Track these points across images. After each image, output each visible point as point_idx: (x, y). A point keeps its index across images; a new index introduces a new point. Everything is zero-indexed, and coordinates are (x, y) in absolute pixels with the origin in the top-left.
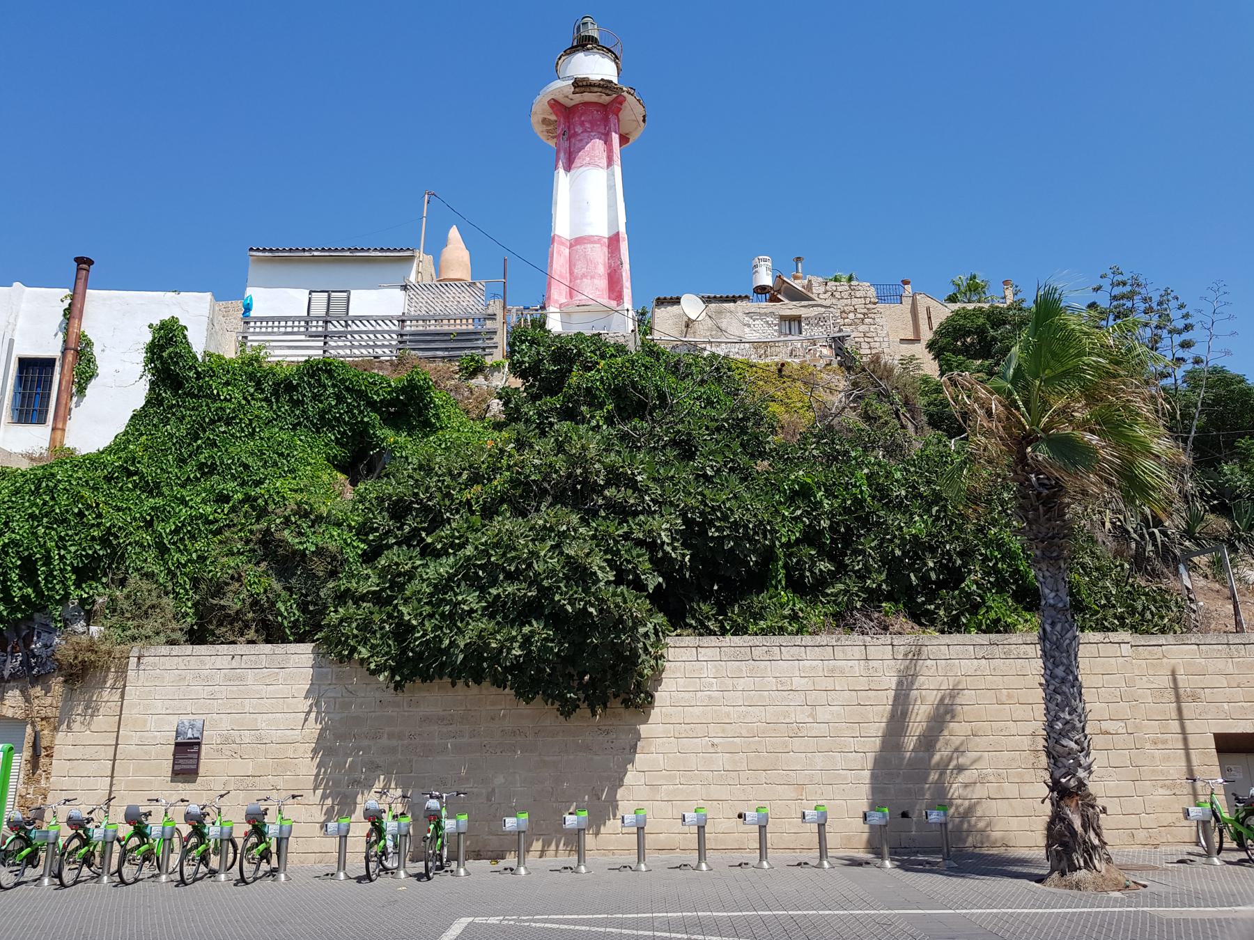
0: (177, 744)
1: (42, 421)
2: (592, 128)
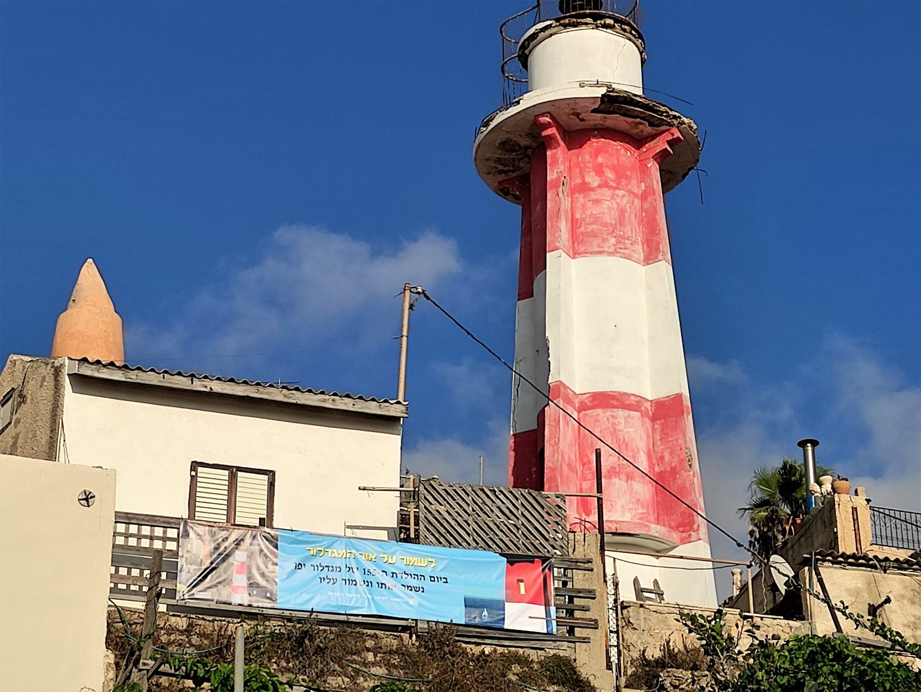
2: (618, 180)
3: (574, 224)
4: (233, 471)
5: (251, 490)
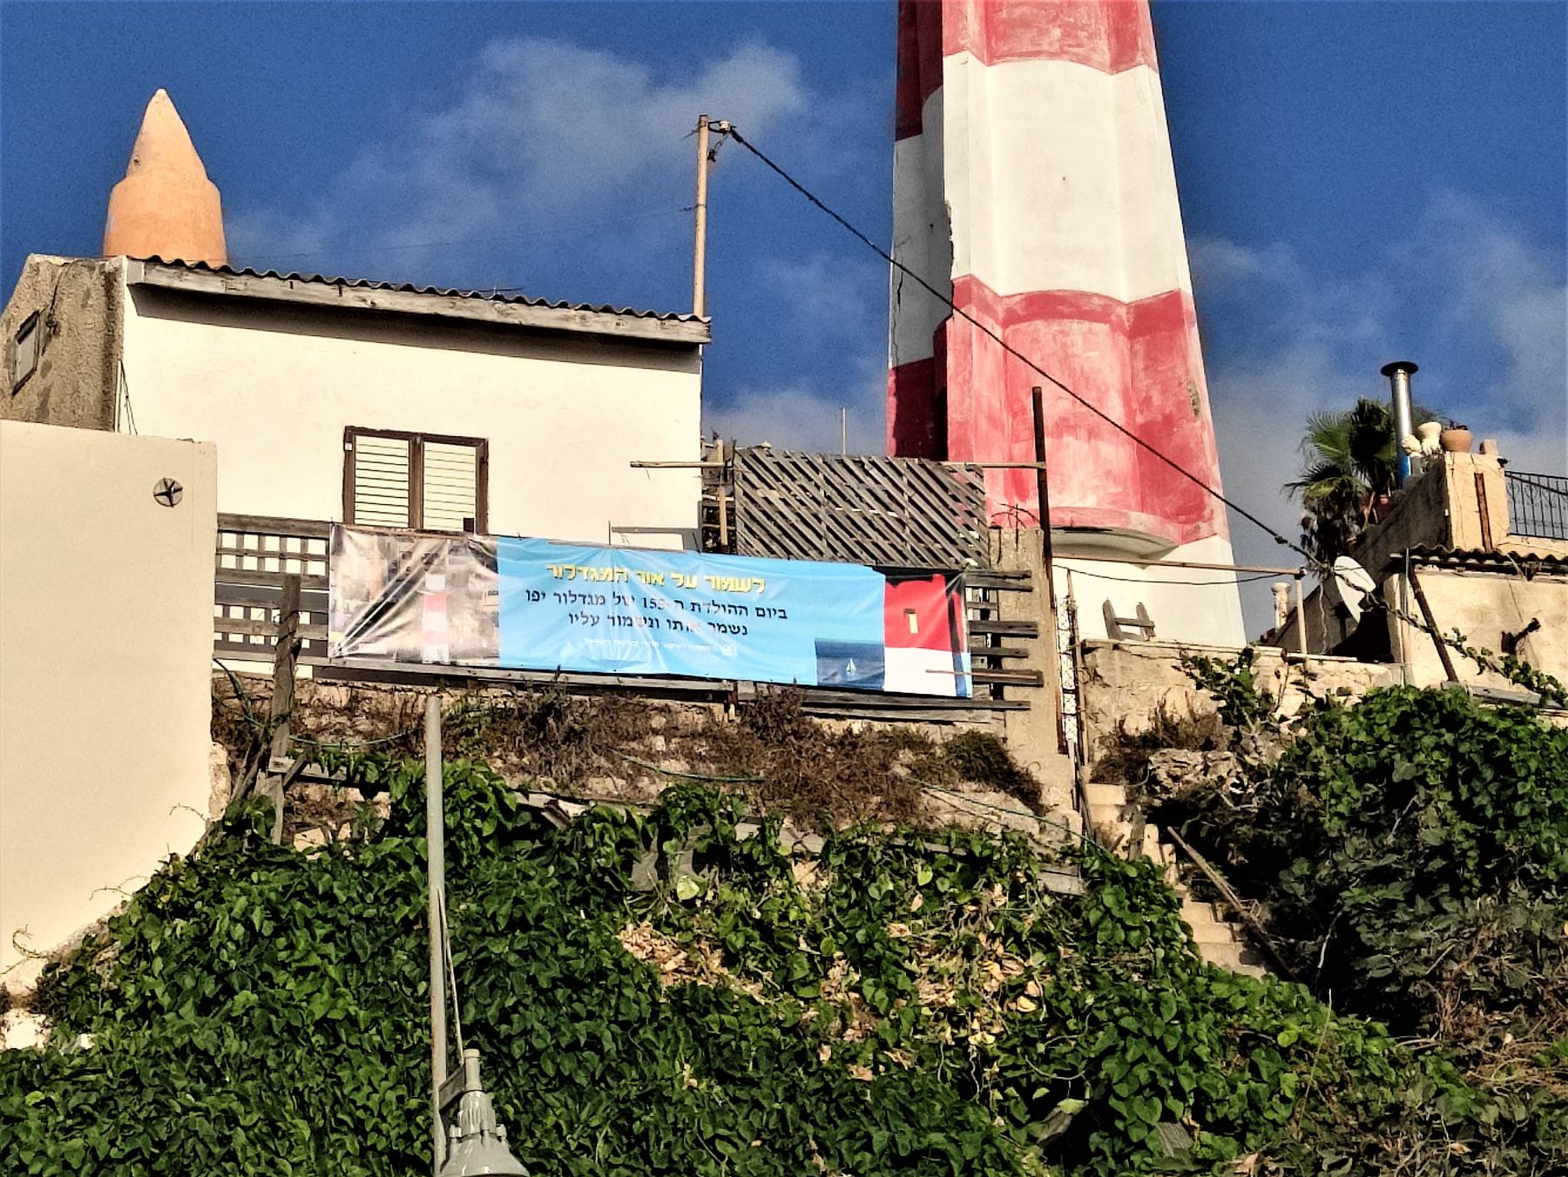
4: (417, 442)
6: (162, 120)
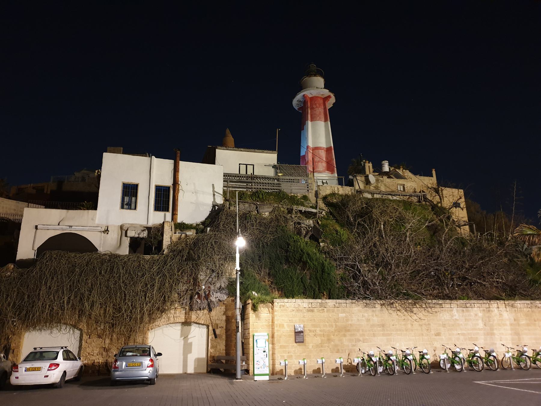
0: (295, 332)
1: (168, 211)
3: (311, 115)
4: (246, 165)
5: (250, 168)
6: (228, 131)
